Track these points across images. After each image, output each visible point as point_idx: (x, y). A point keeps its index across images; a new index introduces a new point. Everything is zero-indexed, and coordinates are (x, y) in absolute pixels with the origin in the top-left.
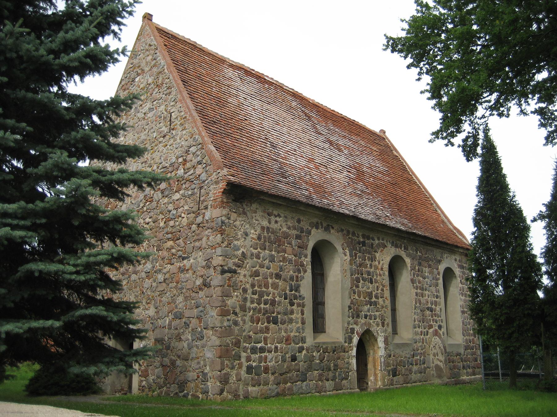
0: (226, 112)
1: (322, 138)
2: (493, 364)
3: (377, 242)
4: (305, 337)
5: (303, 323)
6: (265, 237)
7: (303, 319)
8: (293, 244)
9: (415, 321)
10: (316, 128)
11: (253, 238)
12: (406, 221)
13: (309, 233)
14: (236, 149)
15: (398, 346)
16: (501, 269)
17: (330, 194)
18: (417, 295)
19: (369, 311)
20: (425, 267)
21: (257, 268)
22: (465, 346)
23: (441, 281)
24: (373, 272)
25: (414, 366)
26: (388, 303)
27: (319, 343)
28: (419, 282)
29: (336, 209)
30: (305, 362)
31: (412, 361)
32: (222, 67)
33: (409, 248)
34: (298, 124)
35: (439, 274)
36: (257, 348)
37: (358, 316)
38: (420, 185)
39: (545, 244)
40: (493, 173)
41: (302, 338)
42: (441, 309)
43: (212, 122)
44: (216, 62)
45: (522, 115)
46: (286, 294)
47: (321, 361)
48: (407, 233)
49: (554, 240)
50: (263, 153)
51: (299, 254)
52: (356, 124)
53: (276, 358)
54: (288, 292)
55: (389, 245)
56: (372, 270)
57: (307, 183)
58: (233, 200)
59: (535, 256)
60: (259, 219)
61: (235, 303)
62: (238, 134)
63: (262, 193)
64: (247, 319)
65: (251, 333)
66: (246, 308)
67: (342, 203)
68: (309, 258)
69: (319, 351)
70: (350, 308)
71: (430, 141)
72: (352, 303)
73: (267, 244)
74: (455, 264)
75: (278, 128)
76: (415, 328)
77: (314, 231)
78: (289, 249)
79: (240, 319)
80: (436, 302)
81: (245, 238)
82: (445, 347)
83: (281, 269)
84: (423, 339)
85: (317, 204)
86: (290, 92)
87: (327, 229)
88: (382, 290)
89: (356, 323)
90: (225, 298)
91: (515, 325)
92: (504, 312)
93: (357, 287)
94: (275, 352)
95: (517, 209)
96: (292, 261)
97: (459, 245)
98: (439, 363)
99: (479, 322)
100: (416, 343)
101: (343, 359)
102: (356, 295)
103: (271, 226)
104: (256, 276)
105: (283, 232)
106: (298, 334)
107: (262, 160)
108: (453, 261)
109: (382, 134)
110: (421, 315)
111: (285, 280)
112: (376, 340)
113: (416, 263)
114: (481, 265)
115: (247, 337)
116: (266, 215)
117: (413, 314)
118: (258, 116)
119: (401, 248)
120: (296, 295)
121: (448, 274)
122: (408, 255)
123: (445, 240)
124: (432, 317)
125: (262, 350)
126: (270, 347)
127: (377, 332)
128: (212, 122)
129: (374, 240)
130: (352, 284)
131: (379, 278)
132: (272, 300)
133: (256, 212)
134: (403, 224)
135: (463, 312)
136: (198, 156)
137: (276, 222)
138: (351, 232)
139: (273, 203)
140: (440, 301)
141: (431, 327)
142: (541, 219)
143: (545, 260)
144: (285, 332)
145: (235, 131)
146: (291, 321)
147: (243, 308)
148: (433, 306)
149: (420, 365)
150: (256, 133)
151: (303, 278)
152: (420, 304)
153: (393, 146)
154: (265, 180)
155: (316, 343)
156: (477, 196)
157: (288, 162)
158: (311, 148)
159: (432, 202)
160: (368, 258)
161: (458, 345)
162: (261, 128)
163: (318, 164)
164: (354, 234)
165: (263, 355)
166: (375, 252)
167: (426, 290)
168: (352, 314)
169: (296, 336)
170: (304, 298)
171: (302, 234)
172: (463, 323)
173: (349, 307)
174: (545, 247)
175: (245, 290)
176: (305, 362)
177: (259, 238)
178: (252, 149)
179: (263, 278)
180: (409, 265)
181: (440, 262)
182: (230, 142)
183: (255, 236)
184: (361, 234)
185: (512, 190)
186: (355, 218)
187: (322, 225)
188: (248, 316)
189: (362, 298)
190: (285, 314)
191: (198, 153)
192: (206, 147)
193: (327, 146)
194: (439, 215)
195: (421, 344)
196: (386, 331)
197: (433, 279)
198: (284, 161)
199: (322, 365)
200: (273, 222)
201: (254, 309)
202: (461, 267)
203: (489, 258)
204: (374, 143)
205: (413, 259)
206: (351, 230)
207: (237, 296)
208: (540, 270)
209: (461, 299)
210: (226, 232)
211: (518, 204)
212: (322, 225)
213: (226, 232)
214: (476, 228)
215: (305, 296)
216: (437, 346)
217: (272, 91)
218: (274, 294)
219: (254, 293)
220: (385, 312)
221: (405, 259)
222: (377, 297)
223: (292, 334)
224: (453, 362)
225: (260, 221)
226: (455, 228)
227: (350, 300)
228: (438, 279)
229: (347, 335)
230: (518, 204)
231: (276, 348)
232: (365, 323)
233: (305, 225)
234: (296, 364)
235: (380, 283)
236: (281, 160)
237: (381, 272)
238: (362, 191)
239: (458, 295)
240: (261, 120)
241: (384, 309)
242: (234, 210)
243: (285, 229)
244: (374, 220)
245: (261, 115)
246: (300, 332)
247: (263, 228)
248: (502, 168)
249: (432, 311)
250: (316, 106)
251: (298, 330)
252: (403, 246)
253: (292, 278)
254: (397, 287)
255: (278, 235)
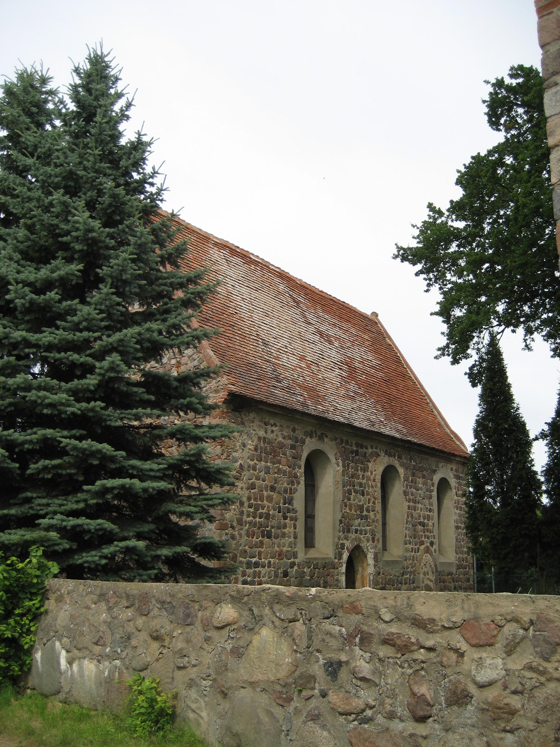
0: (217, 306)
1: (312, 329)
2: (486, 586)
3: (370, 451)
4: (297, 552)
5: (295, 537)
6: (261, 448)
7: (295, 533)
8: (288, 455)
9: (406, 537)
10: (305, 317)
11: (250, 449)
12: (400, 427)
13: (304, 442)
14: (231, 351)
15: (388, 563)
16: (500, 484)
17: (324, 398)
18: (409, 508)
19: (359, 526)
20: (419, 478)
21: (253, 480)
22: (458, 565)
23: (435, 494)
24: (365, 484)
25: (403, 585)
26: (379, 516)
27: (310, 559)
28: (412, 495)
29: (330, 416)
30: (296, 578)
31: (402, 579)
32: (207, 247)
33: (403, 457)
34: (287, 314)
35: (433, 485)
36: (252, 562)
37: (349, 531)
38: (415, 381)
39: (546, 462)
40: (498, 382)
41: (294, 553)
42: (433, 524)
43: (206, 320)
44: (201, 241)
45: (527, 350)
46: (279, 507)
47: (311, 577)
48: (401, 440)
49: (556, 457)
50: (256, 354)
51: (294, 465)
52: (347, 307)
53: (269, 573)
54: (281, 505)
55: (383, 454)
56: (364, 481)
57: (300, 386)
58: (232, 410)
59: (535, 473)
60: (255, 428)
61: (233, 516)
62: (231, 332)
63: (261, 402)
64: (243, 532)
65: (247, 547)
66: (242, 522)
67: (336, 409)
68: (302, 470)
69: (310, 568)
70: (341, 522)
71: (436, 358)
72: (343, 517)
73: (263, 455)
74: (451, 474)
75: (267, 320)
76: (406, 544)
77: (308, 440)
78: (284, 460)
79: (236, 533)
80: (428, 516)
81: (243, 450)
82: (436, 566)
83: (276, 481)
84: (413, 556)
85: (313, 413)
86: (277, 272)
87: (321, 438)
88: (374, 503)
89: (346, 538)
90: (223, 511)
91: (511, 545)
92: (500, 531)
93: (349, 499)
94: (268, 567)
95: (520, 422)
96: (286, 472)
97: (456, 453)
98: (429, 583)
99: (475, 540)
100: (406, 560)
101: (333, 576)
102: (347, 509)
103: (267, 436)
104: (252, 489)
105: (278, 442)
106: (290, 549)
107: (256, 362)
108: (449, 470)
109: (373, 318)
110: (412, 530)
111: (279, 493)
112: (366, 557)
113: (409, 473)
114: (480, 480)
115: (243, 552)
116: (263, 425)
117: (404, 529)
118: (248, 307)
119: (395, 457)
120: (289, 509)
121: (443, 485)
122: (402, 465)
123: (440, 448)
124: (424, 532)
125: (256, 565)
126: (264, 562)
127: (368, 549)
128: (206, 320)
129: (367, 449)
130: (344, 497)
131: (371, 489)
132: (267, 513)
133: (253, 422)
134: (398, 431)
135: (457, 528)
136: (195, 360)
137: (272, 432)
138: (344, 441)
139: (270, 412)
140: (433, 516)
141: (422, 543)
142: (542, 438)
143: (545, 478)
144: (278, 547)
145: (228, 328)
146: (284, 535)
147: (240, 522)
148: (426, 521)
149: (410, 584)
150: (247, 329)
151: (297, 490)
152: (412, 519)
153: (386, 332)
154: (261, 387)
155: (307, 558)
156: (480, 405)
157: (280, 363)
158: (301, 343)
159: (428, 400)
160: (361, 468)
161: (450, 564)
162: (251, 323)
163: (310, 362)
164: (347, 443)
165: (257, 569)
166: (368, 461)
167: (419, 503)
168: (343, 528)
169: (288, 551)
170: (296, 512)
171: (297, 443)
172: (456, 539)
173: (340, 521)
174: (547, 464)
175: (242, 504)
176: (296, 578)
177: (256, 449)
178: (245, 350)
179: (259, 491)
180: (402, 476)
181: (434, 471)
182: (225, 343)
183: (252, 447)
184: (354, 442)
185: (516, 401)
186: (350, 426)
187: (316, 434)
188: (244, 530)
189: (353, 512)
190: (279, 528)
191: (195, 356)
192: (205, 352)
193: (317, 338)
194: (435, 417)
195: (411, 562)
196: (376, 547)
197: (427, 491)
198: (277, 361)
199: (312, 581)
200: (269, 432)
201: (250, 523)
202: (457, 477)
203: (488, 473)
204: (366, 330)
205: (406, 469)
206: (344, 438)
207: (235, 509)
208: (540, 487)
209: (455, 513)
210: (225, 444)
211: (522, 417)
212: (316, 434)
213: (225, 444)
214: (476, 440)
215: (297, 509)
216: (428, 564)
217: (259, 273)
218: (268, 507)
219: (250, 507)
220: (376, 527)
221: (398, 469)
222: (368, 511)
223: (285, 549)
224: (444, 582)
225: (257, 431)
226: (453, 432)
227: (341, 514)
228: (432, 491)
229: (337, 550)
230: (522, 417)
231: (269, 562)
232: (355, 539)
233: (299, 434)
234: (288, 580)
235: (372, 496)
236: (274, 360)
237: (374, 484)
238: (355, 392)
239: (452, 508)
240: (251, 312)
241: (375, 523)
242: (233, 421)
243: (280, 439)
244: (368, 428)
245: (250, 305)
246: (292, 547)
247: (259, 438)
248: (507, 377)
249: (424, 526)
250: (304, 287)
251: (290, 545)
252: (397, 454)
253: (285, 491)
254: (388, 499)
255: (274, 445)
